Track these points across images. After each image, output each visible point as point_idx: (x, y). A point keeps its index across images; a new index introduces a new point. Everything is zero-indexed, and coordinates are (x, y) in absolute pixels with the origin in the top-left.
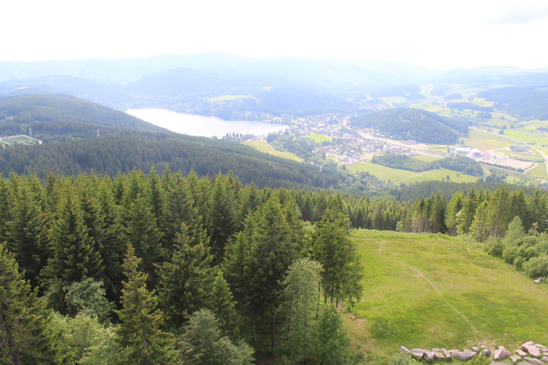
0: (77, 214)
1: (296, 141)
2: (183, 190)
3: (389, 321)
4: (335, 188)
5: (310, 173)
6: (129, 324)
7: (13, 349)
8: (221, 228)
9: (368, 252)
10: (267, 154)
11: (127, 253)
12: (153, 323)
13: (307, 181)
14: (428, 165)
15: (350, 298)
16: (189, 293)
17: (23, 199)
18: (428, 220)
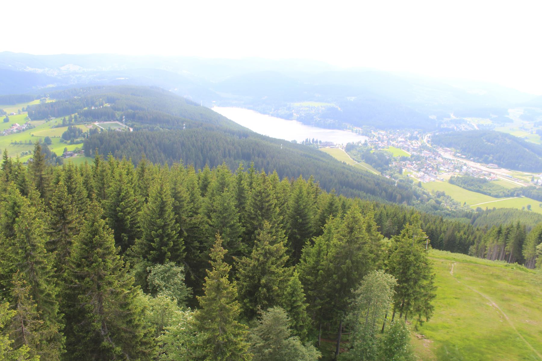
0: (167, 201)
1: (374, 153)
2: (268, 189)
3: (456, 346)
4: (409, 204)
5: (385, 186)
6: (207, 310)
7: (103, 316)
8: (298, 231)
9: (439, 272)
10: (344, 163)
11: (215, 243)
12: (231, 313)
13: (381, 194)
14: (508, 192)
15: (420, 315)
16: (265, 289)
17: (120, 181)
18: (504, 248)
